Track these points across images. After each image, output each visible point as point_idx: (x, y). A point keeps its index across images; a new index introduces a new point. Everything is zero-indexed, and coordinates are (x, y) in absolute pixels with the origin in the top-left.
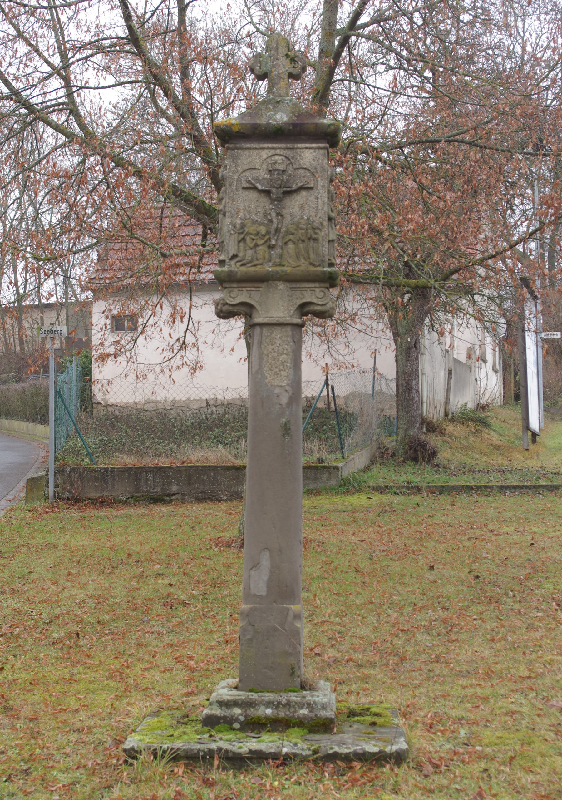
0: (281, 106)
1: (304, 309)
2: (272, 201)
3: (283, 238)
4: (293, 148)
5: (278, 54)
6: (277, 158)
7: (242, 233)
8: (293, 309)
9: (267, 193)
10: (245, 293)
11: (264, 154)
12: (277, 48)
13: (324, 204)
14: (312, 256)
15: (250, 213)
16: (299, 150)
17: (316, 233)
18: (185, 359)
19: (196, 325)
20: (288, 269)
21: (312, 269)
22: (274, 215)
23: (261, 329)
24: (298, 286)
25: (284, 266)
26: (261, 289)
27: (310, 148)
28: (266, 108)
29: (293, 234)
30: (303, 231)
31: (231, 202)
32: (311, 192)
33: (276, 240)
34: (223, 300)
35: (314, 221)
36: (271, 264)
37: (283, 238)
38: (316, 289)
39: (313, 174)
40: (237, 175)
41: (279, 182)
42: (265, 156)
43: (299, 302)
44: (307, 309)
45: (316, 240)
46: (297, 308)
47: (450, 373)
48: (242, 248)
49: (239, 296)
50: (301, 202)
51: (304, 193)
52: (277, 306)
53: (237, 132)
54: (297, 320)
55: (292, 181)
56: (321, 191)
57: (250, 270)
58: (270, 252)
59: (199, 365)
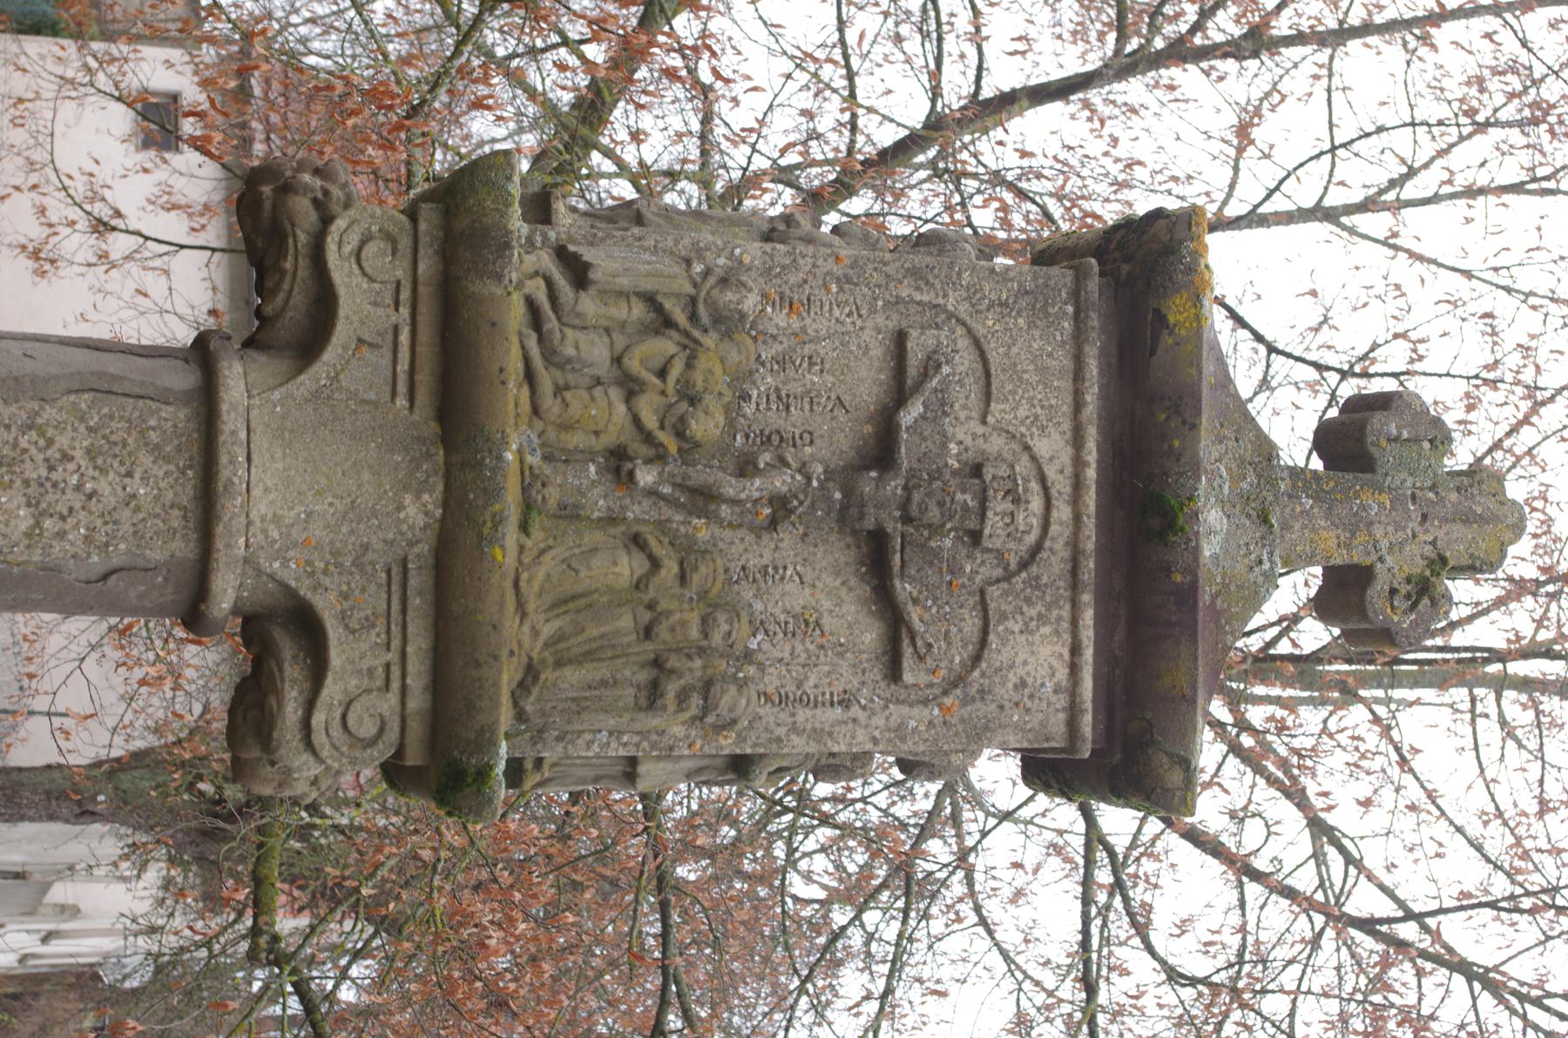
0: (1252, 532)
1: (281, 634)
2: (846, 476)
3: (662, 525)
4: (1075, 585)
5: (1444, 520)
6: (1036, 504)
7: (693, 317)
8: (291, 573)
9: (881, 450)
10: (384, 317)
11: (1052, 446)
12: (1467, 518)
13: (818, 734)
14: (573, 676)
15: (782, 362)
16: (1066, 612)
17: (682, 697)
18: (66, 231)
19: (157, 263)
20: (507, 548)
21: (508, 676)
22: (781, 482)
23: (186, 398)
24: (415, 602)
25: (524, 527)
26: (402, 402)
27: (1074, 669)
28: (1242, 463)
29: (683, 578)
30: (694, 633)
31: (838, 270)
32: (876, 674)
33: (652, 493)
34: (347, 205)
35: (742, 685)
36: (533, 460)
37: (662, 525)
38: (393, 698)
39: (956, 682)
40: (963, 309)
41: (934, 513)
42: (1042, 447)
43: (326, 605)
44: (287, 648)
45: (652, 696)
46: (291, 593)
47: (18, 876)
48: (619, 311)
49: (368, 290)
50: (826, 621)
51: (870, 635)
52: (311, 490)
53: (1161, 318)
54: (226, 592)
55: (931, 575)
56: (879, 721)
57: (511, 343)
58: (591, 455)
59: (47, 267)
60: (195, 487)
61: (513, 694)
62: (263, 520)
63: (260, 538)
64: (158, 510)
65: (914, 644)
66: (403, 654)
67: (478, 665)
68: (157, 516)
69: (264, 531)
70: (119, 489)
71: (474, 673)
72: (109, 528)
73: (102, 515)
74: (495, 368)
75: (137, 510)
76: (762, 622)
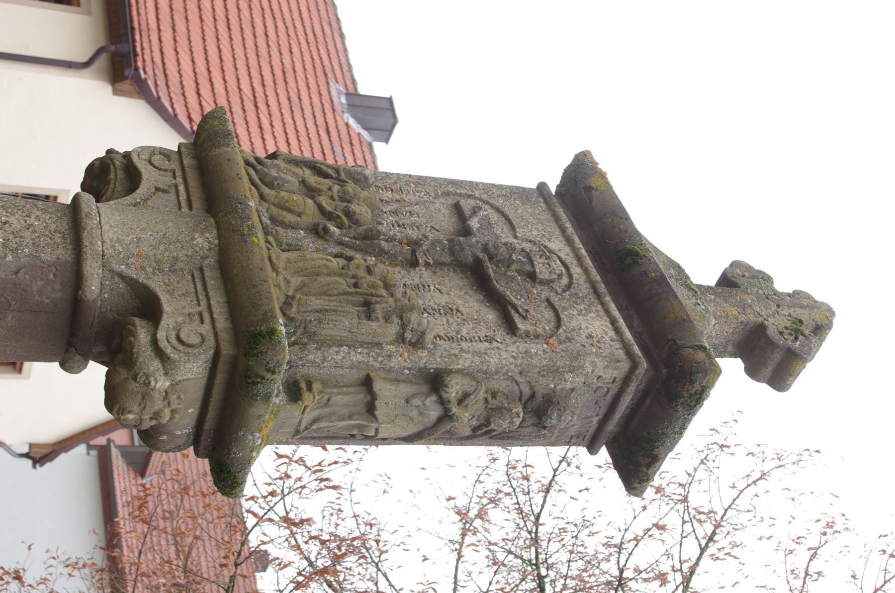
24: (211, 283)
26: (185, 209)
51: (491, 316)
60: (68, 224)
61: (281, 309)
62: (111, 240)
63: (111, 250)
64: (47, 233)
65: (517, 311)
66: (209, 306)
67: (255, 286)
68: (47, 236)
69: (113, 247)
70: (23, 222)
71: (254, 291)
72: (18, 240)
73: (13, 233)
74: (235, 174)
75: (34, 232)
76: (424, 309)
